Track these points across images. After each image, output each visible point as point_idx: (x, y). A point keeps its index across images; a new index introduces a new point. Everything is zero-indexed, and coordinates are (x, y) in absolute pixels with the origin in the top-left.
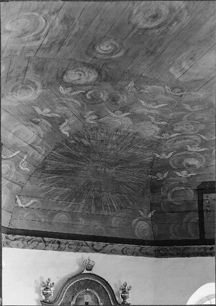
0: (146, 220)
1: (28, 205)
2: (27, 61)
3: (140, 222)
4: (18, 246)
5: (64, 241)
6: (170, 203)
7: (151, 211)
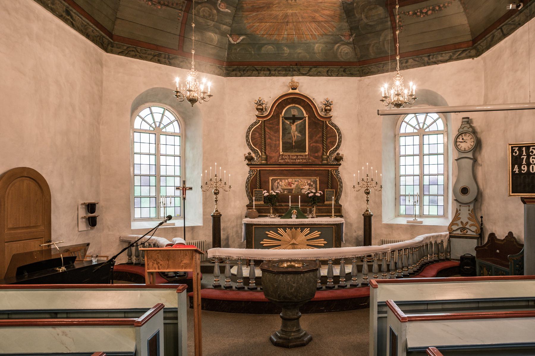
0: (348, 44)
1: (238, 41)
2: (188, 185)
3: (342, 47)
7: (351, 35)
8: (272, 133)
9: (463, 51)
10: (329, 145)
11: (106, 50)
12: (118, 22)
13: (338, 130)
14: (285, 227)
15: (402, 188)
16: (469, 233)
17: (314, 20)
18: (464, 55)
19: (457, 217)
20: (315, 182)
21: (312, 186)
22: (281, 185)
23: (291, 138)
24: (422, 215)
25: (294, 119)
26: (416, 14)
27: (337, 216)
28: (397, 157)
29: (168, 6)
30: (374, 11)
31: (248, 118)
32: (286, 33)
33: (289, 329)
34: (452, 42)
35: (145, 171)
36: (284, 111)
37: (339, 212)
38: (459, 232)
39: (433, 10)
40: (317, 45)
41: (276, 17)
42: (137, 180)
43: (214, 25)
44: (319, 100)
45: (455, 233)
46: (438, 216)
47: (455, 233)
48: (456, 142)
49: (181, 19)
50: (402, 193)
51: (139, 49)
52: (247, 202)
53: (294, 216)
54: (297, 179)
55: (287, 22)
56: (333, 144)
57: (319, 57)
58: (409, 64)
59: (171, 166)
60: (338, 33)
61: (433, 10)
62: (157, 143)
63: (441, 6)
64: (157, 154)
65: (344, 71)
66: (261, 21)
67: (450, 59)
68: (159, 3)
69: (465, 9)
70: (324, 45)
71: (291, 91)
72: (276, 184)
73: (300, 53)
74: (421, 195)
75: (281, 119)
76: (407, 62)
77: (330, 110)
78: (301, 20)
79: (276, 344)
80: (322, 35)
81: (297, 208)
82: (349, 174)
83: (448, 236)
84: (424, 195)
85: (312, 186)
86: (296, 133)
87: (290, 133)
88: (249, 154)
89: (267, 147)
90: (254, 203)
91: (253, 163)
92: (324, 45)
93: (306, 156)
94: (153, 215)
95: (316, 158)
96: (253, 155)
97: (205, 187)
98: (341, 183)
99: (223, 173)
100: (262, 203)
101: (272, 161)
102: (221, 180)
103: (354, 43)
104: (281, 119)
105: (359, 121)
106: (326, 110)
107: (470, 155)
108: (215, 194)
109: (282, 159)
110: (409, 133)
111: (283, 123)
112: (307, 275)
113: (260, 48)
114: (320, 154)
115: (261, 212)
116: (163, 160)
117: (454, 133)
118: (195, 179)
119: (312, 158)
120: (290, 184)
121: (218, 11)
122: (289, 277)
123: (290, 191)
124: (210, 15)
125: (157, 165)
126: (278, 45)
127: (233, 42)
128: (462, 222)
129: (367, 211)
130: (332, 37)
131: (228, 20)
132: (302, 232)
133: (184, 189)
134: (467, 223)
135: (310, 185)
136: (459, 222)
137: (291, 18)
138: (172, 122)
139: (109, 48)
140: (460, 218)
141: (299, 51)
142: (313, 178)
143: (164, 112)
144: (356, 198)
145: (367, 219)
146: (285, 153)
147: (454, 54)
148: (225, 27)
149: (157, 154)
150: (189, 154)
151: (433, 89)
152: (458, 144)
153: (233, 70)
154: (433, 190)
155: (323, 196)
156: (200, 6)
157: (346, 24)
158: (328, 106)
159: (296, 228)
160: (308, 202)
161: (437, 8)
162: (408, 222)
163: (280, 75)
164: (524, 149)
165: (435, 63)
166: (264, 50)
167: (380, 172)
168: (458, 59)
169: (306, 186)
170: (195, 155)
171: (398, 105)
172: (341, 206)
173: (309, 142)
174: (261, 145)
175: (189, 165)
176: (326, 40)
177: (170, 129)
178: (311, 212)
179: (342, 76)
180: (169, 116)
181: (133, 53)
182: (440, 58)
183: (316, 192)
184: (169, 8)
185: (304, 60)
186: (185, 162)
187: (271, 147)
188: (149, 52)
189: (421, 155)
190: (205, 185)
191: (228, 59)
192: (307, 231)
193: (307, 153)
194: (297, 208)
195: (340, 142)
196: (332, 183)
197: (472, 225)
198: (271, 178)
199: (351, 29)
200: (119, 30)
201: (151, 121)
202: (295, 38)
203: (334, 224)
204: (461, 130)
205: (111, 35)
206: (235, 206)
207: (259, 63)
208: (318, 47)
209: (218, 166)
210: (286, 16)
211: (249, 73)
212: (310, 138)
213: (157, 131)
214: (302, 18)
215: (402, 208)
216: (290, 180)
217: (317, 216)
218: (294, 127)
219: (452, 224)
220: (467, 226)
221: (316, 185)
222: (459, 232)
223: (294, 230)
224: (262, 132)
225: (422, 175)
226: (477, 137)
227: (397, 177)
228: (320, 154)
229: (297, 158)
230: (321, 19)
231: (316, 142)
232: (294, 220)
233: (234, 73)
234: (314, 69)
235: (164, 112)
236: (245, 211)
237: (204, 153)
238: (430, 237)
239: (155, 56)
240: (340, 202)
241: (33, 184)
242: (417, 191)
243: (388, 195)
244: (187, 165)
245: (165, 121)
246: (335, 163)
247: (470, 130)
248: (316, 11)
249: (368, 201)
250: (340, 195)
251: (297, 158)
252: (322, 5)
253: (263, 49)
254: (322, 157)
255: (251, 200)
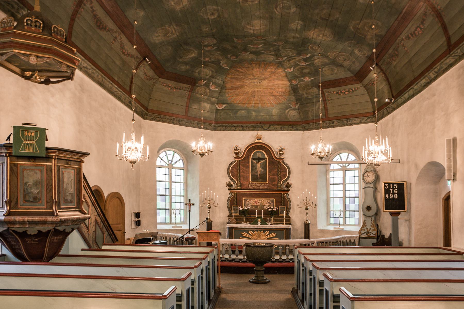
0: (294, 109)
1: (222, 108)
2: (191, 202)
3: (291, 112)
4: (220, 130)
5: (245, 125)
6: (306, 98)
7: (297, 104)
8: (244, 169)
9: (368, 118)
10: (282, 177)
11: (144, 119)
12: (151, 101)
13: (288, 167)
14: (253, 230)
15: (332, 206)
16: (372, 235)
17: (272, 95)
18: (369, 120)
19: (364, 225)
20: (273, 201)
21: (271, 204)
22: (250, 203)
23: (257, 172)
24: (344, 224)
25: (259, 159)
26: (338, 93)
27: (287, 224)
28: (328, 184)
29: (179, 89)
30: (311, 90)
31: (230, 158)
32: (253, 103)
33: (259, 275)
34: (361, 112)
35: (163, 192)
36: (252, 154)
37: (288, 221)
38: (365, 235)
39: (349, 91)
40: (274, 110)
41: (247, 93)
42: (158, 197)
43: (207, 99)
44: (275, 147)
45: (363, 235)
46: (355, 225)
47: (363, 235)
48: (363, 177)
49: (187, 96)
50: (332, 209)
51: (162, 116)
52: (228, 214)
53: (259, 223)
54: (261, 199)
55: (255, 96)
56: (285, 176)
57: (275, 118)
58: (334, 124)
59: (178, 189)
60: (288, 103)
61: (349, 91)
62: (170, 175)
63: (353, 89)
64: (170, 182)
65: (292, 127)
66: (237, 95)
67: (360, 123)
68: (175, 88)
69: (368, 93)
70: (279, 111)
71: (257, 141)
72: (247, 202)
73: (263, 116)
74: (344, 210)
75: (250, 159)
76: (333, 123)
77: (283, 154)
78: (263, 94)
79: (252, 282)
80: (277, 104)
81: (261, 218)
82: (295, 196)
83: (358, 237)
84: (346, 211)
85: (271, 204)
86: (260, 169)
87: (256, 169)
88: (230, 182)
89: (241, 178)
90: (233, 214)
91: (232, 188)
92: (279, 111)
93: (267, 184)
94: (167, 221)
95: (273, 185)
96: (232, 183)
97: (202, 203)
98: (290, 202)
99: (213, 194)
100: (238, 214)
101: (244, 187)
102: (212, 199)
103: (298, 109)
104: (250, 159)
105: (302, 161)
106: (280, 154)
107: (372, 185)
108: (209, 208)
109: (251, 186)
110: (336, 169)
111: (252, 162)
112: (268, 248)
113: (236, 112)
114: (276, 183)
115: (238, 221)
116: (173, 186)
117: (363, 171)
118: (196, 199)
119: (270, 185)
120: (256, 202)
121: (210, 90)
122: (259, 249)
123: (256, 207)
124: (205, 93)
125: (170, 189)
126: (248, 111)
127: (219, 108)
128: (367, 228)
129: (307, 220)
130: (284, 105)
131: (216, 95)
132: (264, 233)
133: (189, 204)
134: (370, 229)
135: (269, 203)
136: (365, 228)
137: (257, 93)
138: (178, 161)
139: (145, 116)
140: (366, 226)
141: (262, 114)
142: (272, 199)
143: (174, 154)
144: (301, 212)
145: (307, 226)
146: (253, 182)
147: (363, 119)
148: (214, 99)
149: (170, 182)
150: (190, 181)
151: (350, 142)
152: (365, 178)
153: (219, 127)
154: (352, 207)
155: (278, 211)
156: (199, 88)
157: (293, 97)
158: (281, 151)
159: (260, 231)
160: (268, 215)
161: (351, 91)
162: (334, 228)
163: (249, 130)
164: (391, 185)
165: (351, 125)
166: (239, 113)
167: (316, 194)
168: (365, 123)
169: (267, 204)
170: (194, 182)
171: (321, 158)
172: (290, 217)
173: (269, 175)
174: (237, 176)
175: (190, 189)
176: (280, 107)
177: (177, 165)
178: (270, 221)
179: (291, 130)
180: (177, 157)
181: (158, 119)
182: (354, 122)
183: (274, 208)
184: (180, 90)
185: (265, 120)
186: (187, 187)
187: (244, 178)
188: (168, 117)
189: (344, 184)
190: (202, 203)
191: (215, 119)
192: (267, 232)
193: (267, 182)
194: (261, 218)
195: (289, 175)
196: (284, 202)
197: (373, 230)
198: (244, 198)
199: (297, 100)
200: (152, 106)
201: (166, 160)
202: (260, 106)
203: (285, 229)
204: (367, 169)
205: (147, 109)
206: (220, 217)
207: (236, 122)
208: (275, 112)
209: (210, 190)
210: (254, 92)
211: (229, 128)
212: (270, 172)
213: (170, 166)
214: (264, 93)
215: (332, 219)
216: (256, 200)
217: (274, 224)
218: (259, 165)
219: (361, 229)
220: (370, 231)
221: (274, 203)
222: (365, 235)
223: (259, 232)
224: (237, 169)
225: (344, 198)
226: (377, 174)
227: (328, 199)
228: (276, 183)
229: (261, 184)
230: (276, 94)
231: (274, 175)
232: (259, 225)
233: (219, 128)
234: (272, 126)
235: (174, 154)
236: (227, 220)
237: (200, 181)
238: (345, 238)
239: (171, 120)
240: (289, 215)
241: (119, 201)
242: (341, 208)
243: (321, 210)
244: (188, 189)
245: (175, 160)
246: (286, 189)
247: (372, 169)
248: (273, 89)
249: (307, 214)
250: (289, 210)
251: (261, 184)
252: (277, 85)
253: (239, 113)
254: (277, 185)
255: (231, 213)
